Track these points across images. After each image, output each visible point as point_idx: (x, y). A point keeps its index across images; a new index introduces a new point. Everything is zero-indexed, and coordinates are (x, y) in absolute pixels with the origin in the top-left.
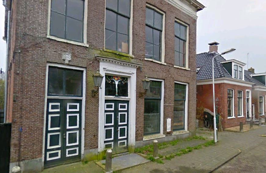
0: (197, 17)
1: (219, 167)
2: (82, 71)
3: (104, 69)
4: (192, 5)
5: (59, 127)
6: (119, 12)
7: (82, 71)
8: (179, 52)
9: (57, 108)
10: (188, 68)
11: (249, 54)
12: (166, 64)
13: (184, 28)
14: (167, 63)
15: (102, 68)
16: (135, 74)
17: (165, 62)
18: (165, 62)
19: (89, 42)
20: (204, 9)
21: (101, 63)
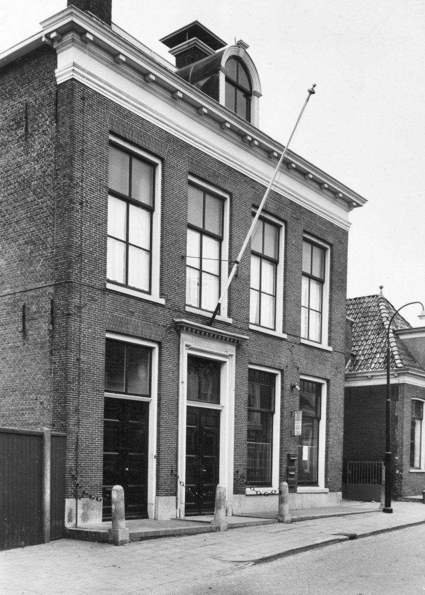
0: (351, 224)
1: (257, 524)
2: (151, 349)
3: (187, 346)
4: (342, 198)
5: (118, 452)
6: (133, 197)
7: (151, 349)
8: (309, 309)
9: (253, 446)
10: (158, 296)
11: (406, 301)
12: (285, 336)
13: (316, 251)
14: (287, 334)
15: (184, 345)
16: (234, 358)
17: (284, 332)
18: (284, 332)
19: (165, 295)
20: (365, 205)
21: (183, 336)
